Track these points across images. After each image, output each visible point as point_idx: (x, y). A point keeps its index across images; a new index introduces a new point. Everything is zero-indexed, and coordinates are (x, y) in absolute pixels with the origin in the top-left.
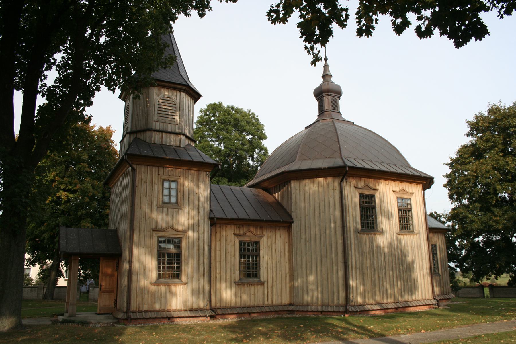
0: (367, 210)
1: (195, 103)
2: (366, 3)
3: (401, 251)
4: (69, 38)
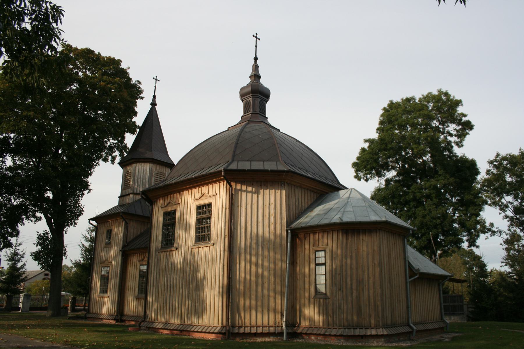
0: (202, 238)
1: (346, 188)
2: (85, 75)
3: (194, 266)
4: (76, 147)
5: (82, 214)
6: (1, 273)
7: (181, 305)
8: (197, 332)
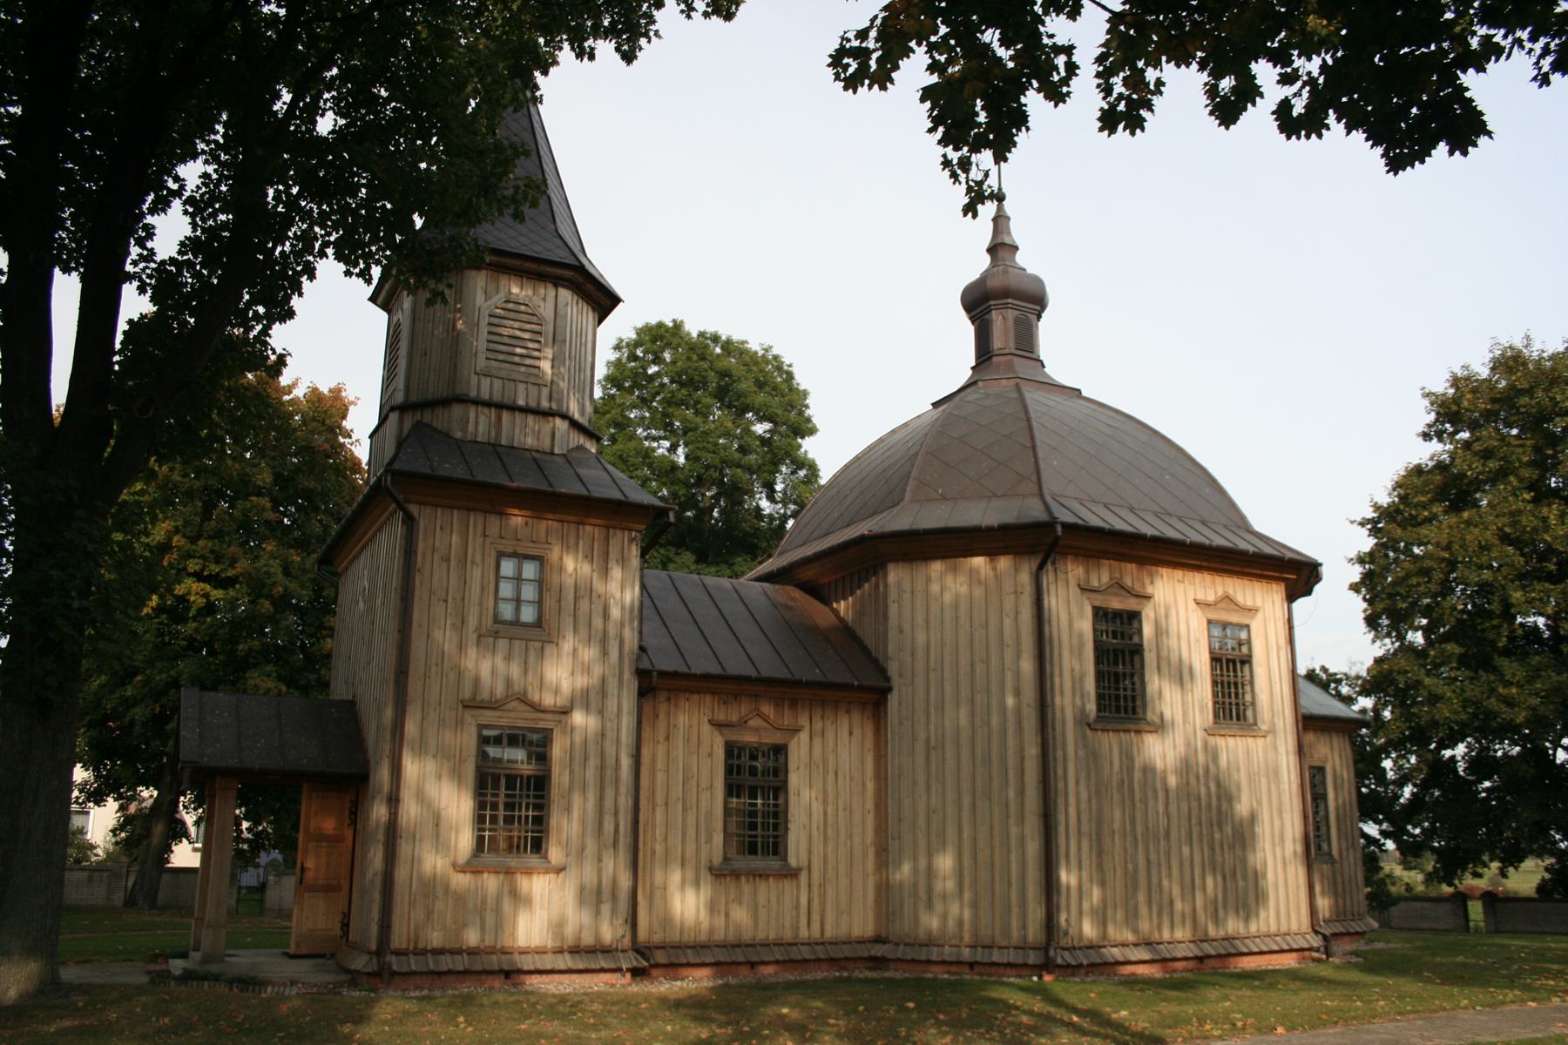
3: (1218, 784)
5: (291, 314)
6: (257, 3)
7: (1189, 889)
8: (1252, 953)
